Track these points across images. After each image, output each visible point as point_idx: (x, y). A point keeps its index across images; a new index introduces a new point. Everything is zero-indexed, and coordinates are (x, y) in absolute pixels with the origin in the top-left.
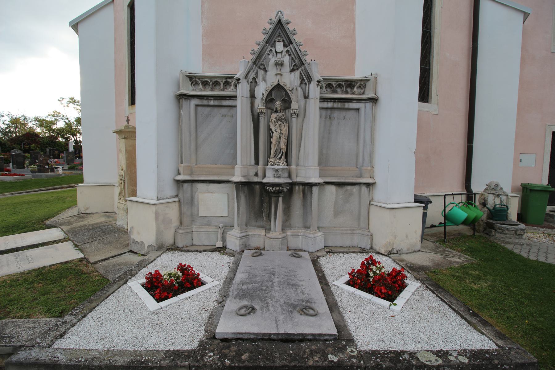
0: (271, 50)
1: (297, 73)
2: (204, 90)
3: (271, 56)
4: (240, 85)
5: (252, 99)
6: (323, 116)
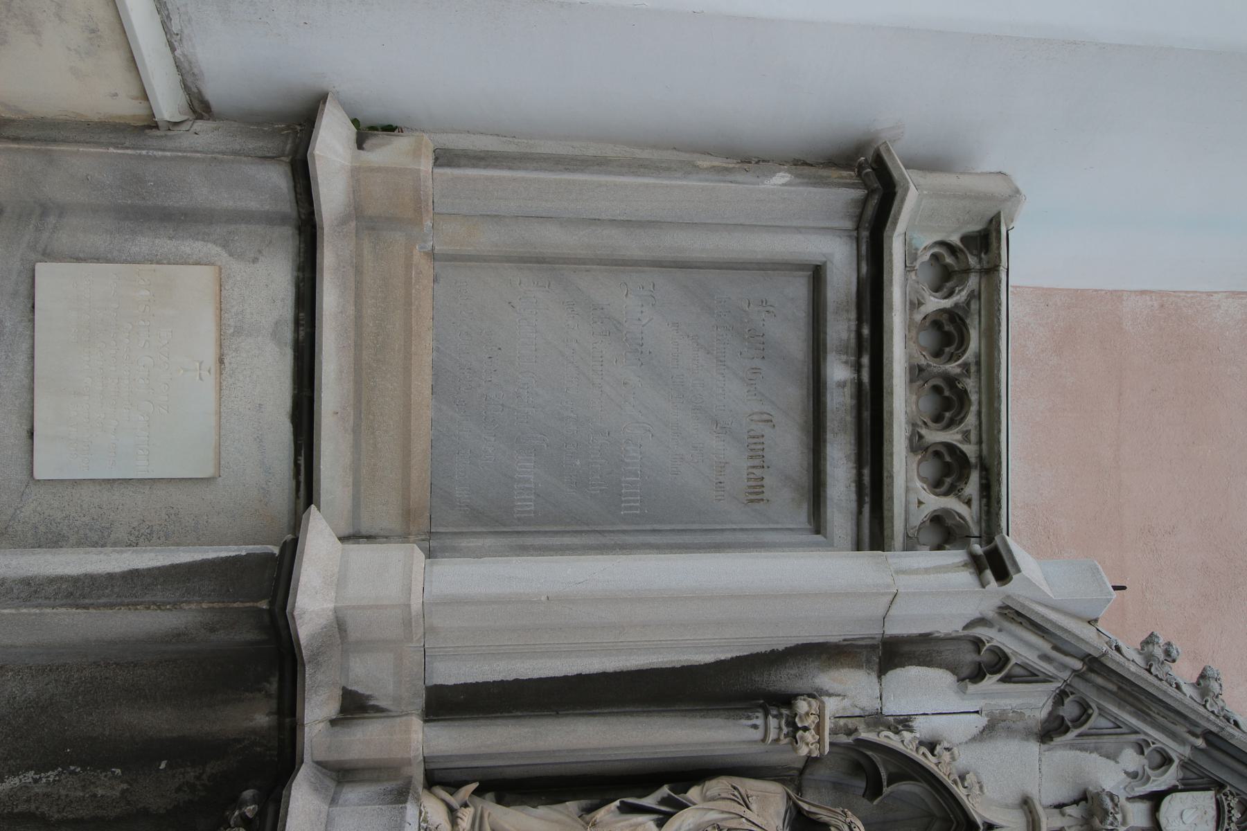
0: (1166, 761)
2: (910, 325)
3: (1131, 760)
4: (966, 577)
5: (873, 647)
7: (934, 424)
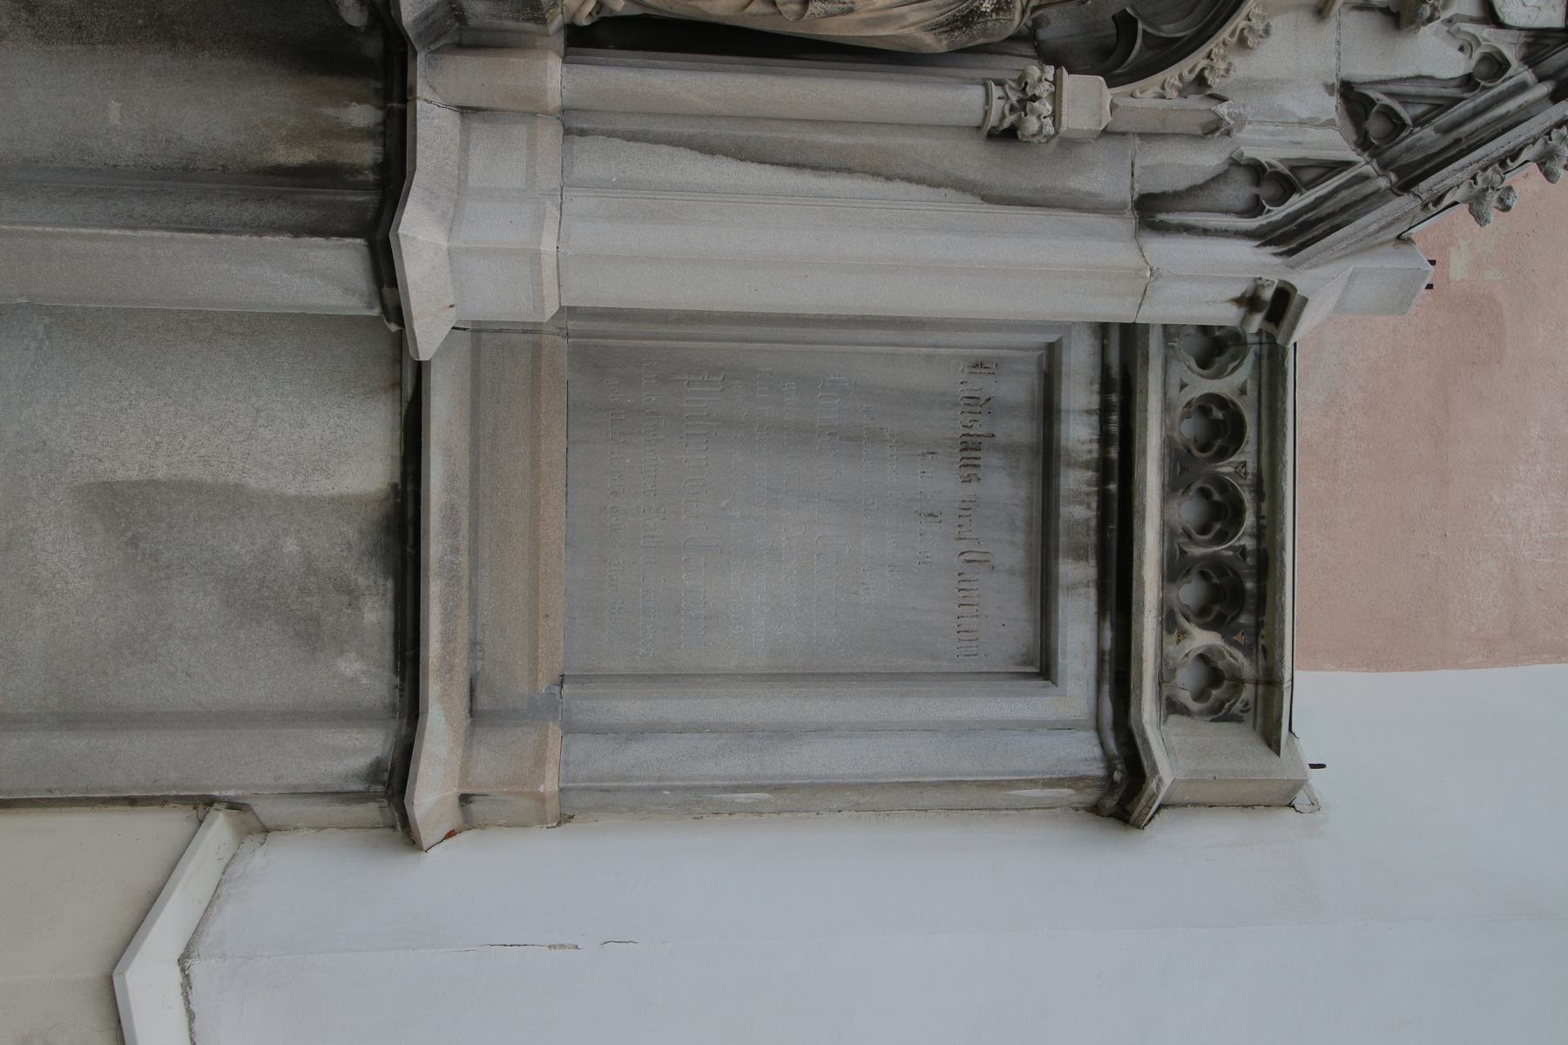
1: (1335, 143)
6: (984, 385)
7: (1194, 703)
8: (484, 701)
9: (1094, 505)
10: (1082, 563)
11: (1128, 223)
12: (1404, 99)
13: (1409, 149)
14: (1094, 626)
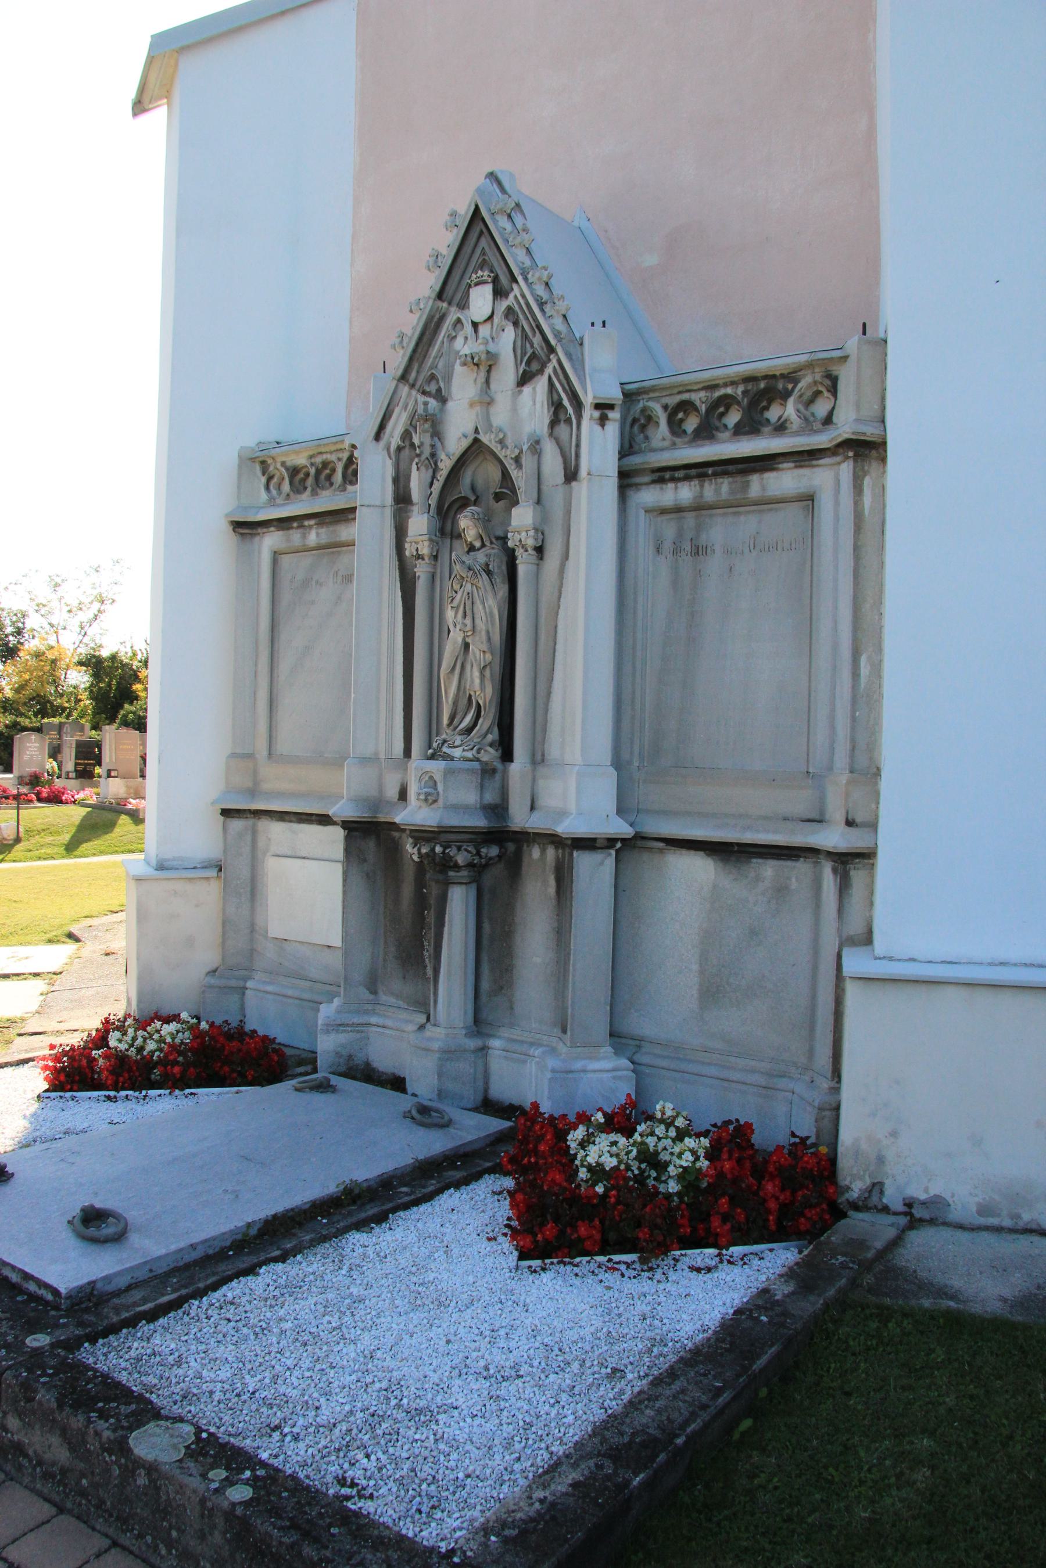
1: (541, 385)
6: (667, 546)
8: (817, 817)
9: (721, 480)
10: (751, 484)
11: (574, 484)
12: (524, 354)
13: (542, 349)
14: (784, 472)
